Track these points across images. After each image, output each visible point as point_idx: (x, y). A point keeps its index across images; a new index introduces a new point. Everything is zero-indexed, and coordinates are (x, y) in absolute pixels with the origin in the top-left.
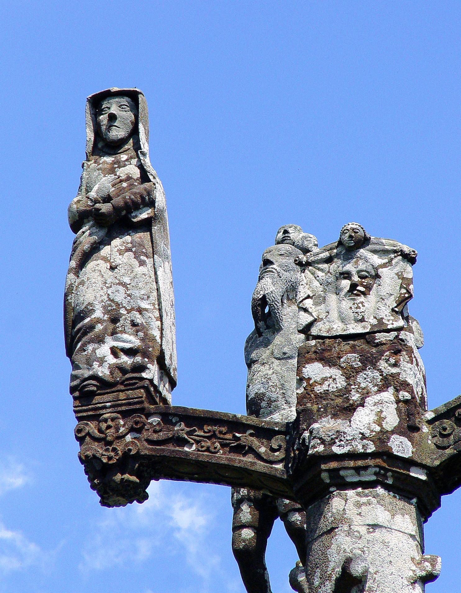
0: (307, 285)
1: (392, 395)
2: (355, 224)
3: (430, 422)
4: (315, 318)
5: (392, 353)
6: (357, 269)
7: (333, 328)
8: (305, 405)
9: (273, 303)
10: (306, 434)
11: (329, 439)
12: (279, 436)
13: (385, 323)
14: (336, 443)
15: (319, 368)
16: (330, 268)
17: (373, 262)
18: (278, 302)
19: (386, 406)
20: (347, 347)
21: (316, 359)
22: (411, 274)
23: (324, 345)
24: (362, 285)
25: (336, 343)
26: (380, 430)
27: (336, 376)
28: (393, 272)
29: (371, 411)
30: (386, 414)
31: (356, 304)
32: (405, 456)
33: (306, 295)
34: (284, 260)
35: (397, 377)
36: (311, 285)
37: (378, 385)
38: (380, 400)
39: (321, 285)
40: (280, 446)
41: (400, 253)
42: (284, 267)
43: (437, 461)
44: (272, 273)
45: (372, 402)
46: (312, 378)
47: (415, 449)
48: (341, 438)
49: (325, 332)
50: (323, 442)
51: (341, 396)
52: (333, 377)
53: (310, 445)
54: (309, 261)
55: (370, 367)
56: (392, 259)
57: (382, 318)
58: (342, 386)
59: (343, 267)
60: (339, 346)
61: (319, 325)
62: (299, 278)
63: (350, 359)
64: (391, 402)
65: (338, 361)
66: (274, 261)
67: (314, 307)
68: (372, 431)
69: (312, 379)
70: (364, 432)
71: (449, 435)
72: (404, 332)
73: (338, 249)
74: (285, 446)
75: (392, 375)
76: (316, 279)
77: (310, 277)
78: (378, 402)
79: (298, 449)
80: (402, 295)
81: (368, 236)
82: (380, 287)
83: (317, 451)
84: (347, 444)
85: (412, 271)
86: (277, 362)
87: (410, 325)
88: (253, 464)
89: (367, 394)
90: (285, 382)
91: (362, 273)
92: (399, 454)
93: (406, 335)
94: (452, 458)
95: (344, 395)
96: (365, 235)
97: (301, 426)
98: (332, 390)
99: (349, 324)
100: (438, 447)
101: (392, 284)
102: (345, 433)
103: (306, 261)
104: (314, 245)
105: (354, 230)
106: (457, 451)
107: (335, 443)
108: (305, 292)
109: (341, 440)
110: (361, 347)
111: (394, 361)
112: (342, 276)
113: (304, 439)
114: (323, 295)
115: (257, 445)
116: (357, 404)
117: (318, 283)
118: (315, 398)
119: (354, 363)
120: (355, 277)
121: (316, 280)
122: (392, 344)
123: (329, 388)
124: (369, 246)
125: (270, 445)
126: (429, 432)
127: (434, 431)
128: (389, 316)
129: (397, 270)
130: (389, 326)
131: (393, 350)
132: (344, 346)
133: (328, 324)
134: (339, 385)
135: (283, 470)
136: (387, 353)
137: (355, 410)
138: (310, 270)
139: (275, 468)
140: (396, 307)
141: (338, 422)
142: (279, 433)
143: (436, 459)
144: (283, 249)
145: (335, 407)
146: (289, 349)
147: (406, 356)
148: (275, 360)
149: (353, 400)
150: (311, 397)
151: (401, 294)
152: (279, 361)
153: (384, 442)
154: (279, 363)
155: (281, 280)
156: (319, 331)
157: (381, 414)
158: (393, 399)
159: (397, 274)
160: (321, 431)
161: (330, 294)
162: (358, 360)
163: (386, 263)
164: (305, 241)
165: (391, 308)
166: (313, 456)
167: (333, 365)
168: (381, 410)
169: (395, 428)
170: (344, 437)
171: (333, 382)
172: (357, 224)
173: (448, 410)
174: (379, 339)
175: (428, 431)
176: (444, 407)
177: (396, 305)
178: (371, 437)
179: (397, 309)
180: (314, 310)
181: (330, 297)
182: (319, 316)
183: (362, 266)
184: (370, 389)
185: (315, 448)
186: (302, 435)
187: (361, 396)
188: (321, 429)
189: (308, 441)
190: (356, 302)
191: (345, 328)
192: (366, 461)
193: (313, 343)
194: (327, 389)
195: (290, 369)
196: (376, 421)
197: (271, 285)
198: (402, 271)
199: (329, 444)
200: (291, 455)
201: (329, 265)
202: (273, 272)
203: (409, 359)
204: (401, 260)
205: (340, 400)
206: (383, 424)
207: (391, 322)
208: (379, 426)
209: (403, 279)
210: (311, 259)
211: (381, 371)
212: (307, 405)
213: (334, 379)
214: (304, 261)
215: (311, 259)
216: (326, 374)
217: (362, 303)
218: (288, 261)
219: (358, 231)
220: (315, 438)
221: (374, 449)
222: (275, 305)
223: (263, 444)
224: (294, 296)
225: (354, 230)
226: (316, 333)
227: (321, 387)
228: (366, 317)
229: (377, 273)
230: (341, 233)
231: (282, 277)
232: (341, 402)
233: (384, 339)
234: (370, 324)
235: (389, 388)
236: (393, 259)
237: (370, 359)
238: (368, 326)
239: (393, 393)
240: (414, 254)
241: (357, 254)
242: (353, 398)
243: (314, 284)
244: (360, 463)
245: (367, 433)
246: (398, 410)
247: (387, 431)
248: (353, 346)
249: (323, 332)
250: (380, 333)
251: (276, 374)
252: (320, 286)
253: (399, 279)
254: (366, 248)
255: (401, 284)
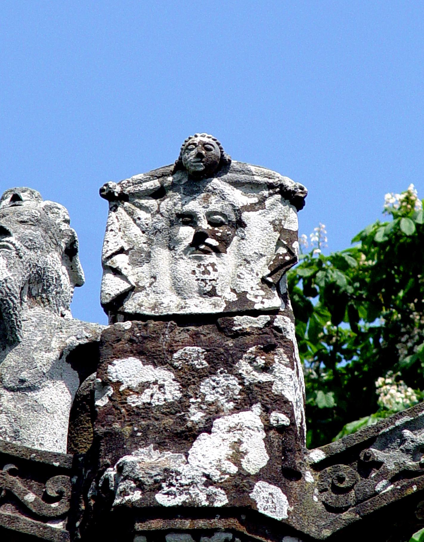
0: (120, 231)
1: (259, 418)
2: (207, 135)
3: (317, 467)
4: (132, 285)
5: (261, 349)
6: (207, 210)
7: (163, 303)
8: (111, 425)
9: (8, 298)
10: (111, 472)
11: (151, 481)
12: (60, 476)
13: (251, 301)
14: (163, 488)
15: (136, 366)
16: (161, 206)
17: (234, 201)
18: (15, 297)
19: (247, 434)
20: (185, 336)
21: (132, 352)
22: (295, 224)
23: (147, 331)
24: (214, 237)
25: (166, 327)
26: (237, 472)
27: (164, 381)
28: (265, 218)
29: (223, 440)
30: (247, 447)
31: (202, 267)
32: (276, 518)
33: (118, 248)
34: (28, 231)
35: (269, 389)
36: (126, 232)
37: (236, 399)
38: (239, 423)
39: (143, 232)
40: (61, 494)
41: (278, 189)
42: (27, 242)
43: (327, 530)
44: (6, 250)
45: (224, 426)
46: (125, 383)
47: (293, 507)
48: (171, 481)
49: (149, 308)
50: (140, 485)
51: (172, 414)
52: (159, 383)
53: (118, 490)
54: (125, 192)
55: (222, 369)
56: (264, 199)
57: (244, 292)
58: (173, 398)
59: (183, 205)
60: (171, 334)
61: (139, 297)
62: (49, 262)
63: (190, 355)
64: (256, 429)
65: (169, 357)
66: (11, 231)
67: (130, 267)
68: (224, 473)
69: (123, 384)
70: (211, 474)
71: (347, 490)
72: (282, 316)
73: (175, 176)
74: (70, 494)
75: (260, 385)
76: (135, 222)
77: (125, 219)
78: (235, 427)
79: (93, 497)
80: (280, 257)
81: (227, 157)
82: (244, 241)
83: (129, 501)
84: (182, 491)
85: (297, 220)
86: (8, 395)
87: (289, 307)
88: (12, 520)
89: (217, 413)
90: (21, 427)
91: (215, 217)
92: (268, 513)
93: (286, 322)
94: (352, 526)
95: (176, 412)
96: (222, 156)
97: (101, 460)
98: (157, 403)
99: (190, 298)
100: (329, 508)
101: (263, 238)
102: (178, 473)
103: (119, 192)
104: (64, 221)
105: (206, 146)
106: (360, 516)
107: (160, 488)
108: (116, 242)
109: (171, 485)
110: (209, 336)
111: (264, 362)
112: (181, 220)
113: (107, 480)
114: (145, 249)
115: (22, 489)
116: (200, 428)
117: (139, 229)
118: (128, 415)
119: (196, 362)
120: (203, 222)
121: (135, 225)
122: (260, 334)
123: (153, 400)
124: (229, 174)
125: (44, 490)
126: (314, 483)
127: (322, 481)
128: (257, 289)
129: (272, 216)
130: (256, 304)
131: (262, 344)
132: (179, 333)
133: (153, 297)
134: (169, 397)
135: (63, 532)
136: (253, 349)
137: (195, 437)
138: (126, 207)
139: (51, 528)
140: (269, 276)
141: (166, 456)
142: (60, 471)
143: (325, 527)
144: (26, 213)
145: (162, 431)
146: (29, 375)
147: (285, 356)
148: (6, 391)
149: (192, 421)
150: (121, 413)
151: (279, 255)
152: (12, 393)
153: (244, 491)
154: (11, 397)
155: (22, 262)
156: (138, 307)
157: (240, 446)
158: (259, 423)
159: (272, 223)
160: (138, 467)
161: (159, 248)
162: (203, 357)
163: (255, 204)
164: (49, 213)
165: (260, 276)
166: (122, 507)
167: (161, 363)
168: (239, 439)
169: (262, 470)
170: (177, 480)
171: (160, 390)
172: (210, 136)
173: (347, 449)
174: (240, 325)
175: (313, 480)
176: (342, 444)
177: (269, 272)
178: (221, 483)
179: (270, 279)
180: (131, 273)
181: (159, 253)
182: (138, 282)
183: (215, 205)
184: (222, 405)
185: (126, 495)
186: (103, 474)
187: (205, 416)
188: (138, 464)
189: (113, 483)
190: (202, 263)
191: (183, 304)
192: (212, 521)
193: (128, 325)
194: (149, 401)
195: (30, 407)
196: (232, 456)
197: (5, 268)
198: (280, 218)
199: (151, 490)
200: (80, 507)
201: (159, 202)
202: (8, 247)
203: (288, 360)
204: (280, 200)
205: (171, 420)
206: (242, 463)
207: (260, 299)
208: (235, 465)
209: (282, 231)
210: (128, 189)
211: (240, 377)
212: (114, 426)
213: (162, 386)
214: (117, 192)
215: (128, 189)
216: (147, 377)
217: (213, 265)
218: (34, 233)
219: (211, 147)
220: (126, 478)
221: (227, 501)
222: (10, 302)
223: (30, 488)
224: (40, 291)
225: (206, 146)
226: (133, 310)
227: (138, 398)
228: (218, 289)
229: (240, 219)
230: (182, 149)
231: (23, 257)
232: (171, 423)
233: (249, 326)
234: (225, 301)
235: (254, 406)
236: (267, 198)
237: (223, 356)
238: (222, 303)
239: (259, 414)
240: (302, 193)
241: (208, 186)
242: (192, 418)
243: (132, 231)
244: (201, 523)
245: (216, 475)
246: (267, 440)
247: (249, 475)
248: (195, 334)
249: (145, 308)
250: (242, 315)
251: (6, 413)
252: (142, 234)
253: (275, 231)
254: (222, 177)
255: (279, 239)
